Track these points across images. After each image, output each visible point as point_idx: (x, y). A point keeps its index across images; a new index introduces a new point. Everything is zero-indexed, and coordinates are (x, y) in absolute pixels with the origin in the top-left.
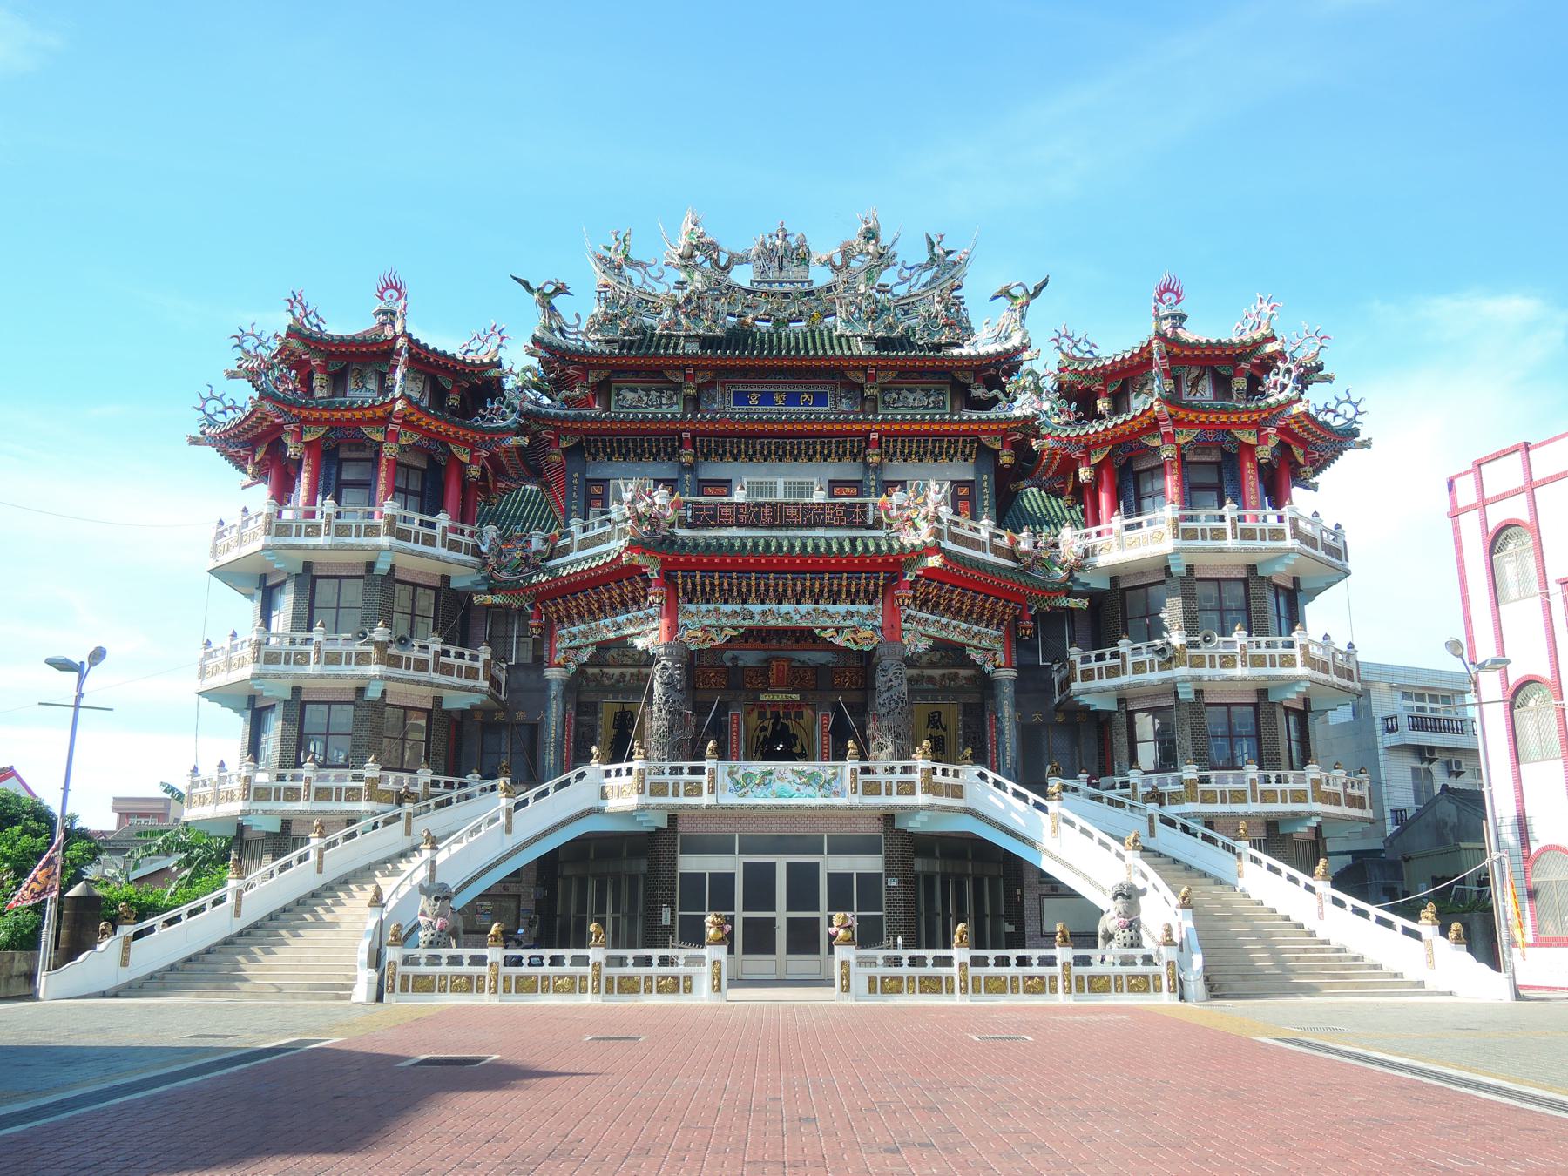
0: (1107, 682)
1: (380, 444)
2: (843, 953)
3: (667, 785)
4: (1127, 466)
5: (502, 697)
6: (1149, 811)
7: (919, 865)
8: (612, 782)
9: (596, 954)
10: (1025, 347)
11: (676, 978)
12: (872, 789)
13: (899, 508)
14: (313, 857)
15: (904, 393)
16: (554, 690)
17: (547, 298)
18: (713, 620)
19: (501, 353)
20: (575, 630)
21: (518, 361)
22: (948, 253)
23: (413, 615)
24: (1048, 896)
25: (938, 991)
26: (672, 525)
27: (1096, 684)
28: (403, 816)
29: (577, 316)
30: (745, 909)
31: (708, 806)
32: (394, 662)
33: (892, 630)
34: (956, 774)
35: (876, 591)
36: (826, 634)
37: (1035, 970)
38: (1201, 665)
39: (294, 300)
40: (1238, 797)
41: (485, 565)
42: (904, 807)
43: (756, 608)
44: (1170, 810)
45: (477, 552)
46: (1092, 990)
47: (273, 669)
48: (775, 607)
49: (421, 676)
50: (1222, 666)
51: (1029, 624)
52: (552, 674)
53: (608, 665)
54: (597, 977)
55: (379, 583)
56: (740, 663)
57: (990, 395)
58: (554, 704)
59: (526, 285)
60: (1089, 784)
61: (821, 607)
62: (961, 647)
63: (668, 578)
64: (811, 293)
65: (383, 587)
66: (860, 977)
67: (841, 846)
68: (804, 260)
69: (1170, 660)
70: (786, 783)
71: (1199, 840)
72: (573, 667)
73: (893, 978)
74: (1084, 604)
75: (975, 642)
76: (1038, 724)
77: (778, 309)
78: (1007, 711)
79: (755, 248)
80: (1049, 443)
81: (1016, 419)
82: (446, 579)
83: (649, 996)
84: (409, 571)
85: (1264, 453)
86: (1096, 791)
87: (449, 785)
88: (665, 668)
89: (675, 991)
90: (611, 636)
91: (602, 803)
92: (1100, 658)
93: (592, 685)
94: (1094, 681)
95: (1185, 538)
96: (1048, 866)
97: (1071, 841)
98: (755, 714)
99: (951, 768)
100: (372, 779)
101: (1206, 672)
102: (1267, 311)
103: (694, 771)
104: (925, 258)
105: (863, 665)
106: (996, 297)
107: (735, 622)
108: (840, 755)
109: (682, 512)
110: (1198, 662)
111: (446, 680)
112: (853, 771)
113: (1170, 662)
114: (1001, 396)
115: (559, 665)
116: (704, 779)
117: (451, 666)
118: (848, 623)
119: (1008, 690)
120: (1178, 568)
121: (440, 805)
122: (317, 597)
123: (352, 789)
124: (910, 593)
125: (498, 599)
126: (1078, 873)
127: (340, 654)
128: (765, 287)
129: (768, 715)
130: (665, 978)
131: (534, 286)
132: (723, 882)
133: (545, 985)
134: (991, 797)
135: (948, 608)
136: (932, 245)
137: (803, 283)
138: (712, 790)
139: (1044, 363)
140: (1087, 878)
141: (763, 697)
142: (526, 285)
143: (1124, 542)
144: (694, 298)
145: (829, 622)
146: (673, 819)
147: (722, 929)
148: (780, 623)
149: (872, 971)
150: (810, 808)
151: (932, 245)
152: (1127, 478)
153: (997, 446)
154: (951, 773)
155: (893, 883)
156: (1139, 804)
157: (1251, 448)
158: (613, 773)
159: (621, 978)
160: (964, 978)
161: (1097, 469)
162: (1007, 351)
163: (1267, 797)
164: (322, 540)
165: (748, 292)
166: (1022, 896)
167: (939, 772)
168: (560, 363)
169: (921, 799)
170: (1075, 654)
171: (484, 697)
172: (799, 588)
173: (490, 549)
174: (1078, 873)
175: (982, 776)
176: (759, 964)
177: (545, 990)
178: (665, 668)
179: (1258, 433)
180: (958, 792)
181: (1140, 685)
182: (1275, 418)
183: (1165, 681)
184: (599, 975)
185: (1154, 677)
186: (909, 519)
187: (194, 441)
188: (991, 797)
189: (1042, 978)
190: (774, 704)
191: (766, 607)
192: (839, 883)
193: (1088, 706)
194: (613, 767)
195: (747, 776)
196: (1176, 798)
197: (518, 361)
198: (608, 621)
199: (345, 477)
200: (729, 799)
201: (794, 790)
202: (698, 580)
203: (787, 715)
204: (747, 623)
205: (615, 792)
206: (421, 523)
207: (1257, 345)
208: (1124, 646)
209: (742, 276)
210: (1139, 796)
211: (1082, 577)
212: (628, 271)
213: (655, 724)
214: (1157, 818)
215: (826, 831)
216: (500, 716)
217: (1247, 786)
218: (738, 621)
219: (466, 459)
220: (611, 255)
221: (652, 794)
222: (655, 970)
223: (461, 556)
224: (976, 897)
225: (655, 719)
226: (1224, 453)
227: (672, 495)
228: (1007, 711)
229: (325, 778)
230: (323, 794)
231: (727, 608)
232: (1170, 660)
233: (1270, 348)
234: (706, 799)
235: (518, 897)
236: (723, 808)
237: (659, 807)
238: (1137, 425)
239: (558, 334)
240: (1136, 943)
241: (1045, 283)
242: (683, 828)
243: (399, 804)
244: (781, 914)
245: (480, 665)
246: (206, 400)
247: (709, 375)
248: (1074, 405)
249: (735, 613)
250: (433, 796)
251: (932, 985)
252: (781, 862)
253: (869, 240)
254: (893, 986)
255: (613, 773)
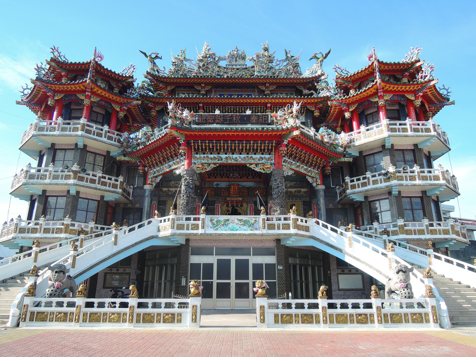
0: (361, 189)
1: (83, 100)
2: (261, 302)
3: (184, 225)
4: (363, 112)
5: (131, 198)
6: (384, 239)
7: (291, 260)
8: (162, 225)
9: (133, 301)
10: (323, 75)
11: (173, 314)
12: (271, 227)
13: (280, 116)
14: (33, 255)
15: (279, 94)
16: (147, 193)
17: (153, 59)
18: (206, 161)
19: (134, 74)
20: (155, 170)
21: (140, 80)
22: (292, 57)
23: (94, 165)
24: (341, 274)
25: (311, 322)
26: (190, 123)
27: (357, 190)
28: (80, 240)
29: (164, 68)
30: (218, 279)
31: (201, 234)
32: (81, 179)
33: (278, 165)
34: (306, 222)
35: (272, 149)
36: (252, 167)
37: (362, 310)
38: (402, 180)
39: (54, 50)
40: (421, 232)
41: (122, 146)
42: (285, 235)
43: (224, 156)
44: (393, 238)
45: (119, 141)
46: (393, 322)
47: (31, 181)
48: (231, 156)
49: (93, 185)
50: (410, 180)
51: (329, 168)
52: (147, 187)
53: (171, 187)
54: (132, 314)
55: (79, 151)
56: (220, 186)
57: (310, 92)
58: (147, 199)
59: (145, 54)
60: (356, 228)
61: (250, 156)
62: (304, 175)
63: (188, 144)
64: (247, 68)
65: (83, 152)
66: (270, 314)
67: (259, 252)
68: (244, 58)
69: (389, 178)
70: (235, 225)
71: (408, 250)
72: (154, 184)
73: (288, 315)
74: (351, 160)
75: (309, 174)
76: (331, 208)
77: (235, 73)
78: (322, 201)
79: (227, 55)
80: (334, 103)
81: (321, 98)
82: (108, 152)
83: (158, 324)
84: (93, 148)
85: (418, 103)
86: (360, 231)
87: (102, 229)
88: (186, 179)
89: (173, 321)
90: (168, 170)
91: (158, 234)
92: (358, 180)
93: (164, 194)
94: (356, 190)
95: (392, 131)
96: (348, 259)
97: (357, 250)
98: (225, 205)
99: (304, 219)
100: (67, 225)
101: (404, 182)
102: (416, 52)
103: (195, 219)
104: (284, 58)
105: (265, 179)
106: (311, 59)
107: (215, 162)
108: (257, 212)
109: (194, 118)
110: (401, 179)
111: (103, 187)
112: (263, 219)
113: (388, 179)
114: (314, 92)
115: (149, 184)
116: (200, 223)
117: (106, 183)
118: (261, 162)
119: (322, 193)
120: (388, 145)
121: (97, 236)
122: (56, 156)
123: (58, 229)
124: (286, 149)
125: (127, 159)
126: (363, 262)
127: (59, 176)
128: (230, 67)
129: (230, 206)
130: (167, 314)
131: (148, 55)
132: (209, 267)
133: (105, 318)
134: (321, 231)
135: (299, 159)
136: (287, 53)
137: (243, 65)
138: (203, 227)
139: (331, 79)
140: (367, 264)
141: (228, 199)
142: (145, 54)
143: (364, 136)
144: (206, 64)
145: (253, 162)
146: (187, 240)
147: (198, 289)
148: (233, 162)
149: (276, 311)
150: (245, 235)
151: (287, 53)
152: (365, 115)
153: (313, 109)
154: (304, 221)
155: (280, 268)
156: (378, 235)
157: (412, 101)
158: (163, 221)
159: (145, 314)
160: (325, 315)
161: (352, 112)
162: (316, 77)
163: (432, 232)
164: (56, 133)
165: (225, 68)
166: (330, 274)
167: (299, 220)
168: (156, 80)
169: (292, 231)
170: (348, 179)
171: (120, 196)
172: (241, 147)
173: (124, 140)
174: (363, 262)
175: (318, 223)
176: (223, 303)
177: (105, 321)
178: (186, 179)
179: (415, 96)
180: (307, 229)
181: (376, 189)
182: (423, 88)
183: (387, 187)
184: (133, 313)
185: (384, 184)
186: (285, 119)
187: (18, 103)
188: (321, 231)
189: (366, 315)
190: (232, 202)
191: (227, 156)
192: (257, 267)
193: (353, 199)
194: (163, 219)
195: (218, 221)
196: (395, 233)
197: (140, 80)
198: (166, 165)
199: (72, 115)
200: (210, 231)
201: (238, 228)
202: (200, 144)
203: (237, 206)
204: (220, 162)
205: (162, 229)
206: (96, 128)
207: (413, 64)
208: (368, 174)
209: (223, 64)
210: (378, 233)
211: (349, 151)
212: (185, 62)
213: (181, 202)
214: (387, 241)
215: (252, 245)
216: (130, 206)
217: (424, 228)
218: (216, 161)
219: (118, 110)
220: (180, 57)
221: (178, 228)
222: (163, 310)
223: (113, 142)
224: (307, 274)
225: (181, 201)
226: (400, 104)
227: (190, 112)
228: (322, 201)
229: (48, 224)
230: (47, 231)
231: (212, 156)
232: (389, 178)
233: (418, 64)
234: (200, 231)
235: (129, 274)
236: (207, 235)
237: (180, 235)
238: (369, 93)
239: (157, 73)
240: (410, 296)
241: (329, 52)
242: (191, 244)
243: (79, 235)
244: (233, 281)
245: (118, 183)
246: (25, 89)
247: (210, 87)
248: (342, 91)
249: (215, 158)
250: (94, 232)
251: (308, 319)
252: (233, 259)
253: (265, 51)
254: (287, 320)
255: (163, 221)
